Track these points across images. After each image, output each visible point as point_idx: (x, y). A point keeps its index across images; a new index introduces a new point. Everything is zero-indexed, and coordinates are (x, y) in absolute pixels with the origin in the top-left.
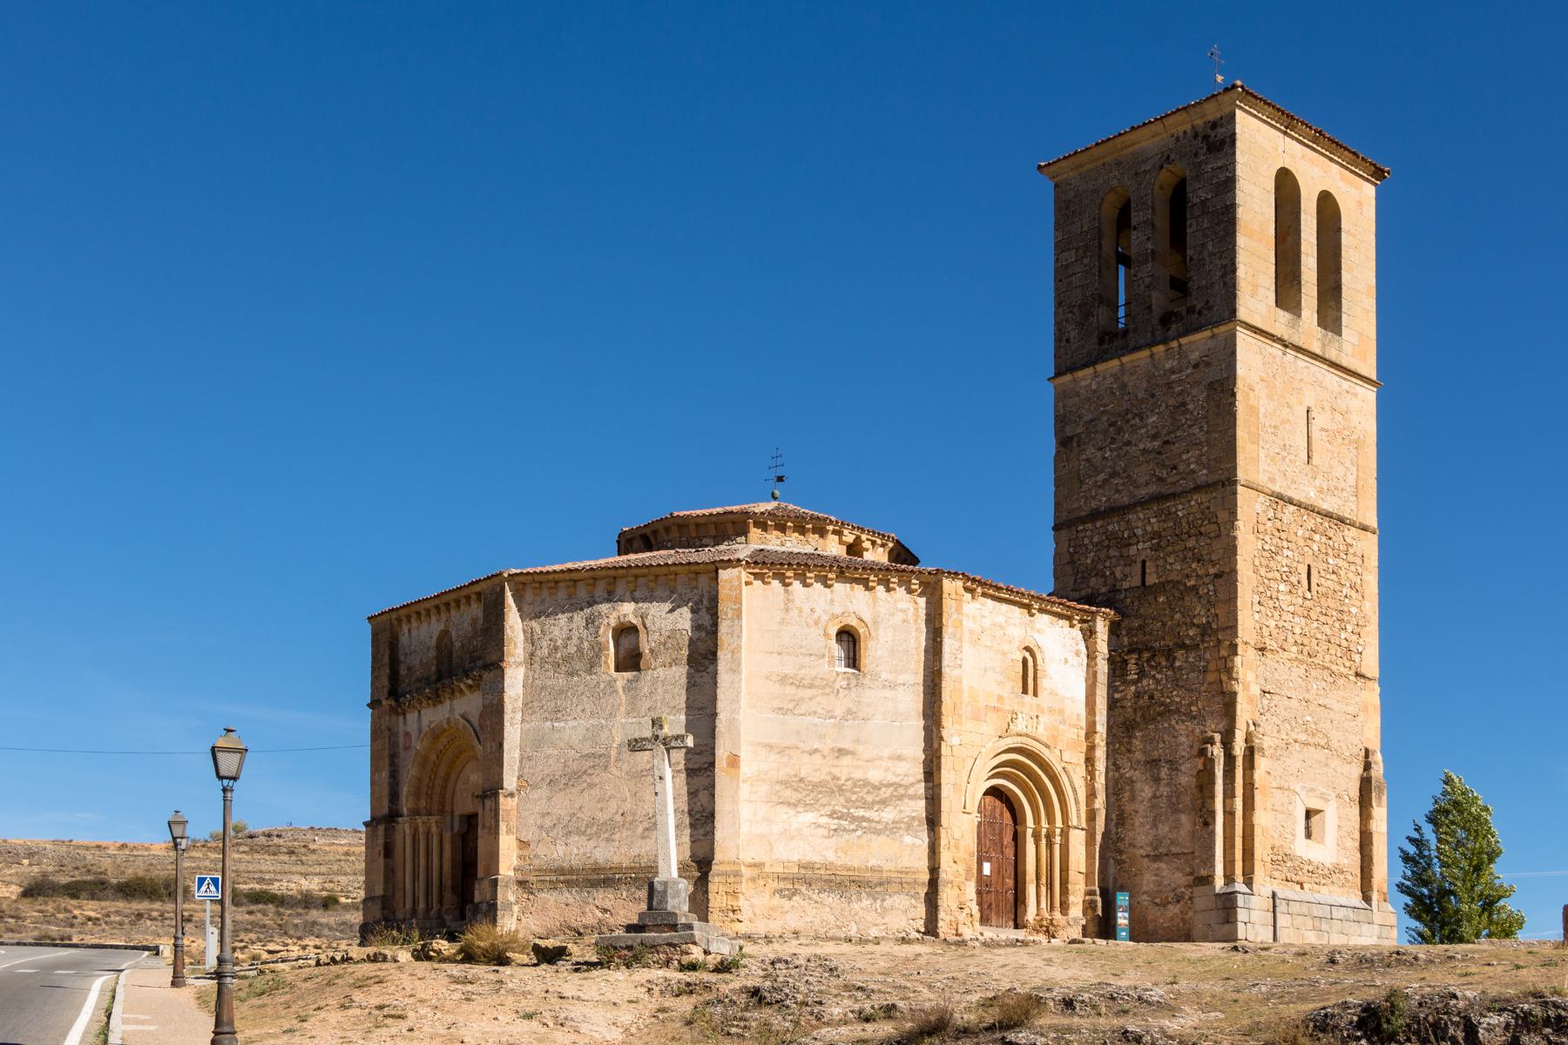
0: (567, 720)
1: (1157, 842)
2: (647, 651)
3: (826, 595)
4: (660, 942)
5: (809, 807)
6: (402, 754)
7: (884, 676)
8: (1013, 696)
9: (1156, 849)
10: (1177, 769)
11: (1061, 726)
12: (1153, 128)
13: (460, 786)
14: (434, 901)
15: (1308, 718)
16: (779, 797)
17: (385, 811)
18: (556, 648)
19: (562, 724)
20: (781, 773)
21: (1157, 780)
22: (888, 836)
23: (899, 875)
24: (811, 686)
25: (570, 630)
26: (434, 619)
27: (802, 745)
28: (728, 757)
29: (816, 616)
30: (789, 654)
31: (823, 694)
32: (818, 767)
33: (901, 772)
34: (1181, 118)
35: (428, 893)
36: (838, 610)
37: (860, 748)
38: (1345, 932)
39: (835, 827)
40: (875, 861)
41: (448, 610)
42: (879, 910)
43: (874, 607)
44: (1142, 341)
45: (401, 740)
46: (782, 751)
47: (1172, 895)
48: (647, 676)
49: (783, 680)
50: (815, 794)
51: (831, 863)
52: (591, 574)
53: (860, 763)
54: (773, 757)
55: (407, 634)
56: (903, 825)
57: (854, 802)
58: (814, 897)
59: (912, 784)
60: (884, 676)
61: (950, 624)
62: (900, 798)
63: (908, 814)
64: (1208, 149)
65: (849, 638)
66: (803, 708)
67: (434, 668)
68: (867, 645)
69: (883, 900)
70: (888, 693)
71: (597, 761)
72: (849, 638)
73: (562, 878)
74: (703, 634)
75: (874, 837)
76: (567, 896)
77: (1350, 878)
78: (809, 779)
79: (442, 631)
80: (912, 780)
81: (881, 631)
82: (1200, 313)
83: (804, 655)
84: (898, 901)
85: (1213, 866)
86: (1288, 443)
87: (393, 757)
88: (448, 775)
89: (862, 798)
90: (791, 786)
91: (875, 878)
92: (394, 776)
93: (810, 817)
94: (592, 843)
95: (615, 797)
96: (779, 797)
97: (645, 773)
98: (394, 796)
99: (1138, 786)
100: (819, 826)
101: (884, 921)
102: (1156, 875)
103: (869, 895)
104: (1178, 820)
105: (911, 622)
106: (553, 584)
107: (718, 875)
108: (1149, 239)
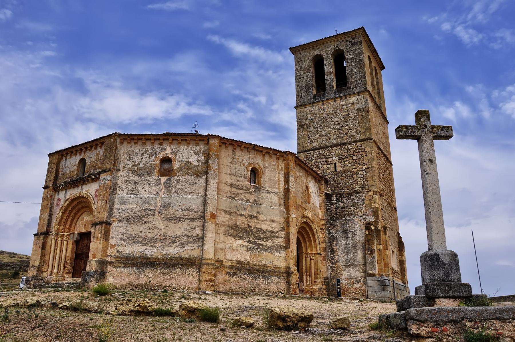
1: (347, 261)
5: (240, 238)
6: (55, 207)
7: (267, 188)
9: (348, 263)
10: (355, 234)
14: (61, 269)
16: (229, 233)
17: (45, 230)
18: (135, 165)
20: (230, 223)
21: (347, 238)
22: (269, 252)
24: (241, 189)
25: (142, 158)
27: (238, 212)
28: (210, 214)
29: (243, 162)
30: (233, 175)
31: (246, 193)
32: (244, 221)
35: (59, 265)
36: (251, 161)
37: (259, 216)
39: (249, 247)
40: (264, 262)
42: (267, 283)
44: (330, 97)
45: (55, 202)
46: (230, 214)
47: (355, 280)
49: (231, 185)
50: (242, 233)
51: (248, 262)
54: (227, 216)
57: (256, 237)
58: (242, 276)
59: (277, 232)
60: (267, 188)
62: (273, 237)
63: (276, 243)
64: (352, 45)
65: (255, 173)
66: (239, 197)
67: (75, 173)
69: (268, 279)
70: (268, 195)
71: (149, 212)
72: (255, 173)
74: (201, 164)
75: (264, 252)
76: (133, 270)
78: (240, 226)
80: (277, 230)
82: (353, 89)
83: (239, 177)
84: (273, 280)
87: (51, 208)
89: (260, 236)
90: (234, 229)
91: (265, 270)
92: (50, 216)
93: (240, 242)
94: (145, 247)
95: (157, 228)
96: (229, 233)
97: (171, 219)
98: (49, 224)
99: (339, 240)
100: (244, 246)
101: (269, 288)
102: (348, 273)
103: (263, 276)
104: (356, 253)
107: (205, 265)
108: (331, 68)
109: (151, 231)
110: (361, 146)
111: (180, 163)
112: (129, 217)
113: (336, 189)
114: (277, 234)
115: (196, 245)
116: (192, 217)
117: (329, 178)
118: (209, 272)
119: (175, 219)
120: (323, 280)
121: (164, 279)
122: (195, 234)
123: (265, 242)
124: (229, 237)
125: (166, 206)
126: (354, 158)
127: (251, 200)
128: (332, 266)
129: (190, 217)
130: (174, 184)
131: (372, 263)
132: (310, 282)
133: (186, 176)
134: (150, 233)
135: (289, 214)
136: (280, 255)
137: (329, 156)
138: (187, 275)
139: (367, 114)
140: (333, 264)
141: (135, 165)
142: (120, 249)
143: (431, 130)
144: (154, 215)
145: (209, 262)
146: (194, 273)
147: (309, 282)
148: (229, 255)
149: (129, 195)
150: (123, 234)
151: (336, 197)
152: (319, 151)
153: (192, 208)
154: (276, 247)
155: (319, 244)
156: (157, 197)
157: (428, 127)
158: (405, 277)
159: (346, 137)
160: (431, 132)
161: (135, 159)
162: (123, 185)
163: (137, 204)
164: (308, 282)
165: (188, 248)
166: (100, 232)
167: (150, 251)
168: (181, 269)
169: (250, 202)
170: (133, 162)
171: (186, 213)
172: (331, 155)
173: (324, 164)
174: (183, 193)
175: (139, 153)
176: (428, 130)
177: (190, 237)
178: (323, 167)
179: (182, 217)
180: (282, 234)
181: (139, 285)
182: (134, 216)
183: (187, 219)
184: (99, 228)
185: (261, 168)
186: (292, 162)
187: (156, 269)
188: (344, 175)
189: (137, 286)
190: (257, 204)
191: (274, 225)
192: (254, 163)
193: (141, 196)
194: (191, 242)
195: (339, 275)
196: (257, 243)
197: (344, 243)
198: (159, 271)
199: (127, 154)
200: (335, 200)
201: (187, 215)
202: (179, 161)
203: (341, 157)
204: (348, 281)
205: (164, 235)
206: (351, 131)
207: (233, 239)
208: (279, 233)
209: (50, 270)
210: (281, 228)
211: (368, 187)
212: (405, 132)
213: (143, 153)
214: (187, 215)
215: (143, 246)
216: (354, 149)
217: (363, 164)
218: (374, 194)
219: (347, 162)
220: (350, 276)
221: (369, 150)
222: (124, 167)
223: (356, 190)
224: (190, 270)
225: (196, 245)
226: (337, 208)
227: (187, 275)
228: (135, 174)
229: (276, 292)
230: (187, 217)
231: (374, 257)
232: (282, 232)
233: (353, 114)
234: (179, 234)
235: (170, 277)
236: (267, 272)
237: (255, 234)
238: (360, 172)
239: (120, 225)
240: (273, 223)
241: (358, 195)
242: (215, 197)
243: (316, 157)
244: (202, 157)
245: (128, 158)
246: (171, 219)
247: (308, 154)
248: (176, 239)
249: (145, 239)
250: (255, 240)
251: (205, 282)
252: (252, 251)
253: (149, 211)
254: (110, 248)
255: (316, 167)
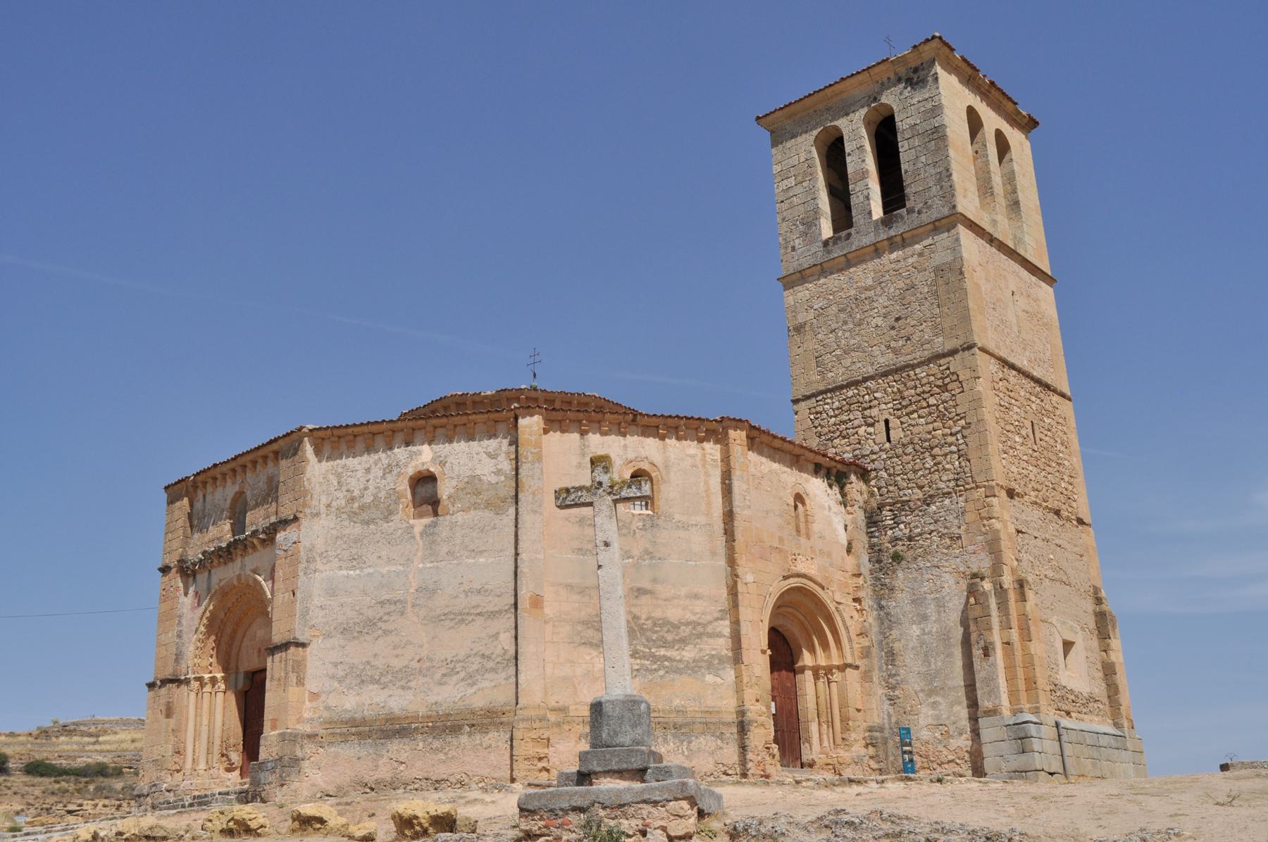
0: (362, 568)
2: (444, 497)
3: (620, 442)
4: (628, 798)
7: (677, 517)
8: (791, 538)
10: (944, 606)
11: (831, 569)
12: (860, 77)
13: (246, 642)
15: (1052, 557)
18: (353, 499)
19: (358, 572)
22: (690, 675)
23: (703, 715)
25: (368, 481)
26: (229, 482)
28: (530, 598)
33: (699, 611)
34: (885, 68)
36: (631, 456)
37: (659, 588)
38: (1110, 759)
41: (245, 472)
42: (686, 753)
43: (664, 452)
46: (582, 591)
48: (444, 521)
52: (390, 426)
53: (660, 602)
54: (576, 597)
55: (201, 500)
56: (703, 664)
59: (710, 622)
60: (677, 517)
61: (737, 468)
62: (700, 636)
63: (708, 652)
68: (659, 488)
69: (690, 742)
71: (393, 607)
73: (353, 730)
74: (503, 478)
75: (677, 676)
77: (1101, 707)
79: (236, 493)
80: (709, 618)
81: (672, 475)
85: (998, 697)
86: (1004, 318)
88: (235, 632)
89: (663, 637)
90: (593, 626)
91: (680, 720)
94: (387, 692)
95: (412, 643)
97: (443, 618)
103: (674, 736)
105: (700, 466)
106: (351, 438)
109: (399, 651)
110: (948, 368)
111: (454, 483)
112: (347, 623)
113: (891, 488)
114: (709, 629)
115: (503, 675)
116: (491, 608)
117: (873, 461)
118: (533, 737)
119: (452, 616)
120: (867, 734)
121: (433, 762)
122: (499, 651)
123: (678, 652)
124: (582, 648)
125: (428, 591)
126: (932, 401)
127: (636, 552)
128: (891, 694)
129: (485, 610)
130: (444, 534)
131: (991, 679)
132: (832, 741)
133: (472, 511)
134: (397, 656)
135: (737, 576)
136: (719, 680)
137: (870, 401)
138: (486, 749)
139: (960, 277)
140: (893, 688)
141: (353, 499)
142: (332, 701)
143: (610, 490)
144: (402, 613)
145: (533, 713)
146: (500, 744)
147: (829, 741)
148: (585, 692)
149: (344, 572)
150: (336, 666)
151: (891, 510)
152: (845, 391)
153: (490, 587)
154: (708, 661)
155: (850, 640)
156: (408, 570)
157: (604, 485)
158: (1119, 709)
159: (909, 348)
160: (609, 493)
161: (353, 484)
162: (329, 548)
163: (365, 592)
164: (825, 737)
165: (485, 684)
166: (283, 666)
167: (398, 702)
168: (470, 734)
169: (633, 558)
170: (348, 491)
171: (475, 599)
172: (875, 398)
173: (859, 427)
174: (466, 554)
175: (359, 467)
176: (604, 491)
177: (489, 658)
178: (857, 433)
179: (466, 611)
180: (725, 627)
181: (377, 782)
182: (357, 621)
183: (479, 614)
184: (281, 657)
185: (659, 470)
186: (738, 442)
187: (414, 740)
188: (910, 449)
189: (373, 786)
190: (651, 558)
191: (699, 606)
192: (639, 459)
193: (371, 570)
194: (493, 670)
195: (909, 717)
196: (655, 656)
197: (918, 633)
198: (421, 744)
199: (332, 474)
200: (890, 520)
201: (478, 606)
202: (452, 478)
203: (900, 404)
204: (934, 733)
205: (430, 660)
206: (921, 328)
207: (592, 651)
208: (715, 624)
209: (189, 765)
210: (721, 611)
211: (971, 476)
212: (565, 499)
213: (369, 468)
214: (478, 606)
215: (382, 689)
216: (932, 378)
217: (957, 415)
218: (988, 494)
219: (915, 415)
220: (938, 719)
221: (968, 376)
222: (329, 506)
223: (942, 485)
224: (490, 735)
225: (503, 675)
226: (897, 539)
227: (486, 749)
228: (355, 519)
229: (712, 774)
230: (478, 611)
231: (994, 665)
232: (721, 622)
233: (923, 280)
234: (462, 653)
235: (447, 758)
236: (687, 724)
237: (649, 634)
238: (950, 439)
239: (328, 646)
240: (698, 602)
241: (947, 502)
242: (538, 556)
243: (838, 409)
244: (505, 463)
245: (336, 484)
246: (443, 618)
247: (817, 401)
248: (457, 666)
249: (387, 672)
250: (650, 649)
251: (526, 762)
252: (644, 676)
253: (390, 604)
254: (310, 701)
255: (838, 437)
